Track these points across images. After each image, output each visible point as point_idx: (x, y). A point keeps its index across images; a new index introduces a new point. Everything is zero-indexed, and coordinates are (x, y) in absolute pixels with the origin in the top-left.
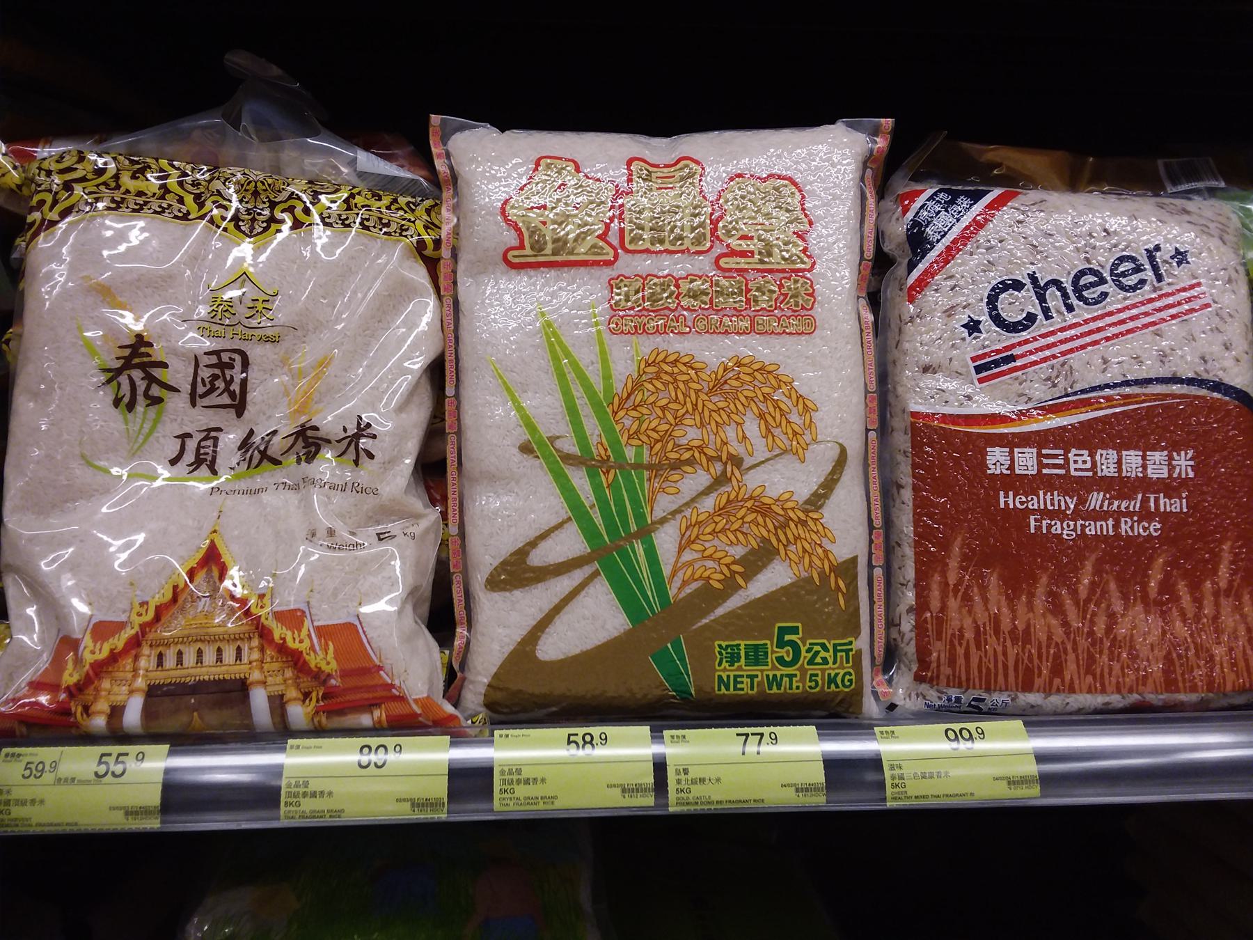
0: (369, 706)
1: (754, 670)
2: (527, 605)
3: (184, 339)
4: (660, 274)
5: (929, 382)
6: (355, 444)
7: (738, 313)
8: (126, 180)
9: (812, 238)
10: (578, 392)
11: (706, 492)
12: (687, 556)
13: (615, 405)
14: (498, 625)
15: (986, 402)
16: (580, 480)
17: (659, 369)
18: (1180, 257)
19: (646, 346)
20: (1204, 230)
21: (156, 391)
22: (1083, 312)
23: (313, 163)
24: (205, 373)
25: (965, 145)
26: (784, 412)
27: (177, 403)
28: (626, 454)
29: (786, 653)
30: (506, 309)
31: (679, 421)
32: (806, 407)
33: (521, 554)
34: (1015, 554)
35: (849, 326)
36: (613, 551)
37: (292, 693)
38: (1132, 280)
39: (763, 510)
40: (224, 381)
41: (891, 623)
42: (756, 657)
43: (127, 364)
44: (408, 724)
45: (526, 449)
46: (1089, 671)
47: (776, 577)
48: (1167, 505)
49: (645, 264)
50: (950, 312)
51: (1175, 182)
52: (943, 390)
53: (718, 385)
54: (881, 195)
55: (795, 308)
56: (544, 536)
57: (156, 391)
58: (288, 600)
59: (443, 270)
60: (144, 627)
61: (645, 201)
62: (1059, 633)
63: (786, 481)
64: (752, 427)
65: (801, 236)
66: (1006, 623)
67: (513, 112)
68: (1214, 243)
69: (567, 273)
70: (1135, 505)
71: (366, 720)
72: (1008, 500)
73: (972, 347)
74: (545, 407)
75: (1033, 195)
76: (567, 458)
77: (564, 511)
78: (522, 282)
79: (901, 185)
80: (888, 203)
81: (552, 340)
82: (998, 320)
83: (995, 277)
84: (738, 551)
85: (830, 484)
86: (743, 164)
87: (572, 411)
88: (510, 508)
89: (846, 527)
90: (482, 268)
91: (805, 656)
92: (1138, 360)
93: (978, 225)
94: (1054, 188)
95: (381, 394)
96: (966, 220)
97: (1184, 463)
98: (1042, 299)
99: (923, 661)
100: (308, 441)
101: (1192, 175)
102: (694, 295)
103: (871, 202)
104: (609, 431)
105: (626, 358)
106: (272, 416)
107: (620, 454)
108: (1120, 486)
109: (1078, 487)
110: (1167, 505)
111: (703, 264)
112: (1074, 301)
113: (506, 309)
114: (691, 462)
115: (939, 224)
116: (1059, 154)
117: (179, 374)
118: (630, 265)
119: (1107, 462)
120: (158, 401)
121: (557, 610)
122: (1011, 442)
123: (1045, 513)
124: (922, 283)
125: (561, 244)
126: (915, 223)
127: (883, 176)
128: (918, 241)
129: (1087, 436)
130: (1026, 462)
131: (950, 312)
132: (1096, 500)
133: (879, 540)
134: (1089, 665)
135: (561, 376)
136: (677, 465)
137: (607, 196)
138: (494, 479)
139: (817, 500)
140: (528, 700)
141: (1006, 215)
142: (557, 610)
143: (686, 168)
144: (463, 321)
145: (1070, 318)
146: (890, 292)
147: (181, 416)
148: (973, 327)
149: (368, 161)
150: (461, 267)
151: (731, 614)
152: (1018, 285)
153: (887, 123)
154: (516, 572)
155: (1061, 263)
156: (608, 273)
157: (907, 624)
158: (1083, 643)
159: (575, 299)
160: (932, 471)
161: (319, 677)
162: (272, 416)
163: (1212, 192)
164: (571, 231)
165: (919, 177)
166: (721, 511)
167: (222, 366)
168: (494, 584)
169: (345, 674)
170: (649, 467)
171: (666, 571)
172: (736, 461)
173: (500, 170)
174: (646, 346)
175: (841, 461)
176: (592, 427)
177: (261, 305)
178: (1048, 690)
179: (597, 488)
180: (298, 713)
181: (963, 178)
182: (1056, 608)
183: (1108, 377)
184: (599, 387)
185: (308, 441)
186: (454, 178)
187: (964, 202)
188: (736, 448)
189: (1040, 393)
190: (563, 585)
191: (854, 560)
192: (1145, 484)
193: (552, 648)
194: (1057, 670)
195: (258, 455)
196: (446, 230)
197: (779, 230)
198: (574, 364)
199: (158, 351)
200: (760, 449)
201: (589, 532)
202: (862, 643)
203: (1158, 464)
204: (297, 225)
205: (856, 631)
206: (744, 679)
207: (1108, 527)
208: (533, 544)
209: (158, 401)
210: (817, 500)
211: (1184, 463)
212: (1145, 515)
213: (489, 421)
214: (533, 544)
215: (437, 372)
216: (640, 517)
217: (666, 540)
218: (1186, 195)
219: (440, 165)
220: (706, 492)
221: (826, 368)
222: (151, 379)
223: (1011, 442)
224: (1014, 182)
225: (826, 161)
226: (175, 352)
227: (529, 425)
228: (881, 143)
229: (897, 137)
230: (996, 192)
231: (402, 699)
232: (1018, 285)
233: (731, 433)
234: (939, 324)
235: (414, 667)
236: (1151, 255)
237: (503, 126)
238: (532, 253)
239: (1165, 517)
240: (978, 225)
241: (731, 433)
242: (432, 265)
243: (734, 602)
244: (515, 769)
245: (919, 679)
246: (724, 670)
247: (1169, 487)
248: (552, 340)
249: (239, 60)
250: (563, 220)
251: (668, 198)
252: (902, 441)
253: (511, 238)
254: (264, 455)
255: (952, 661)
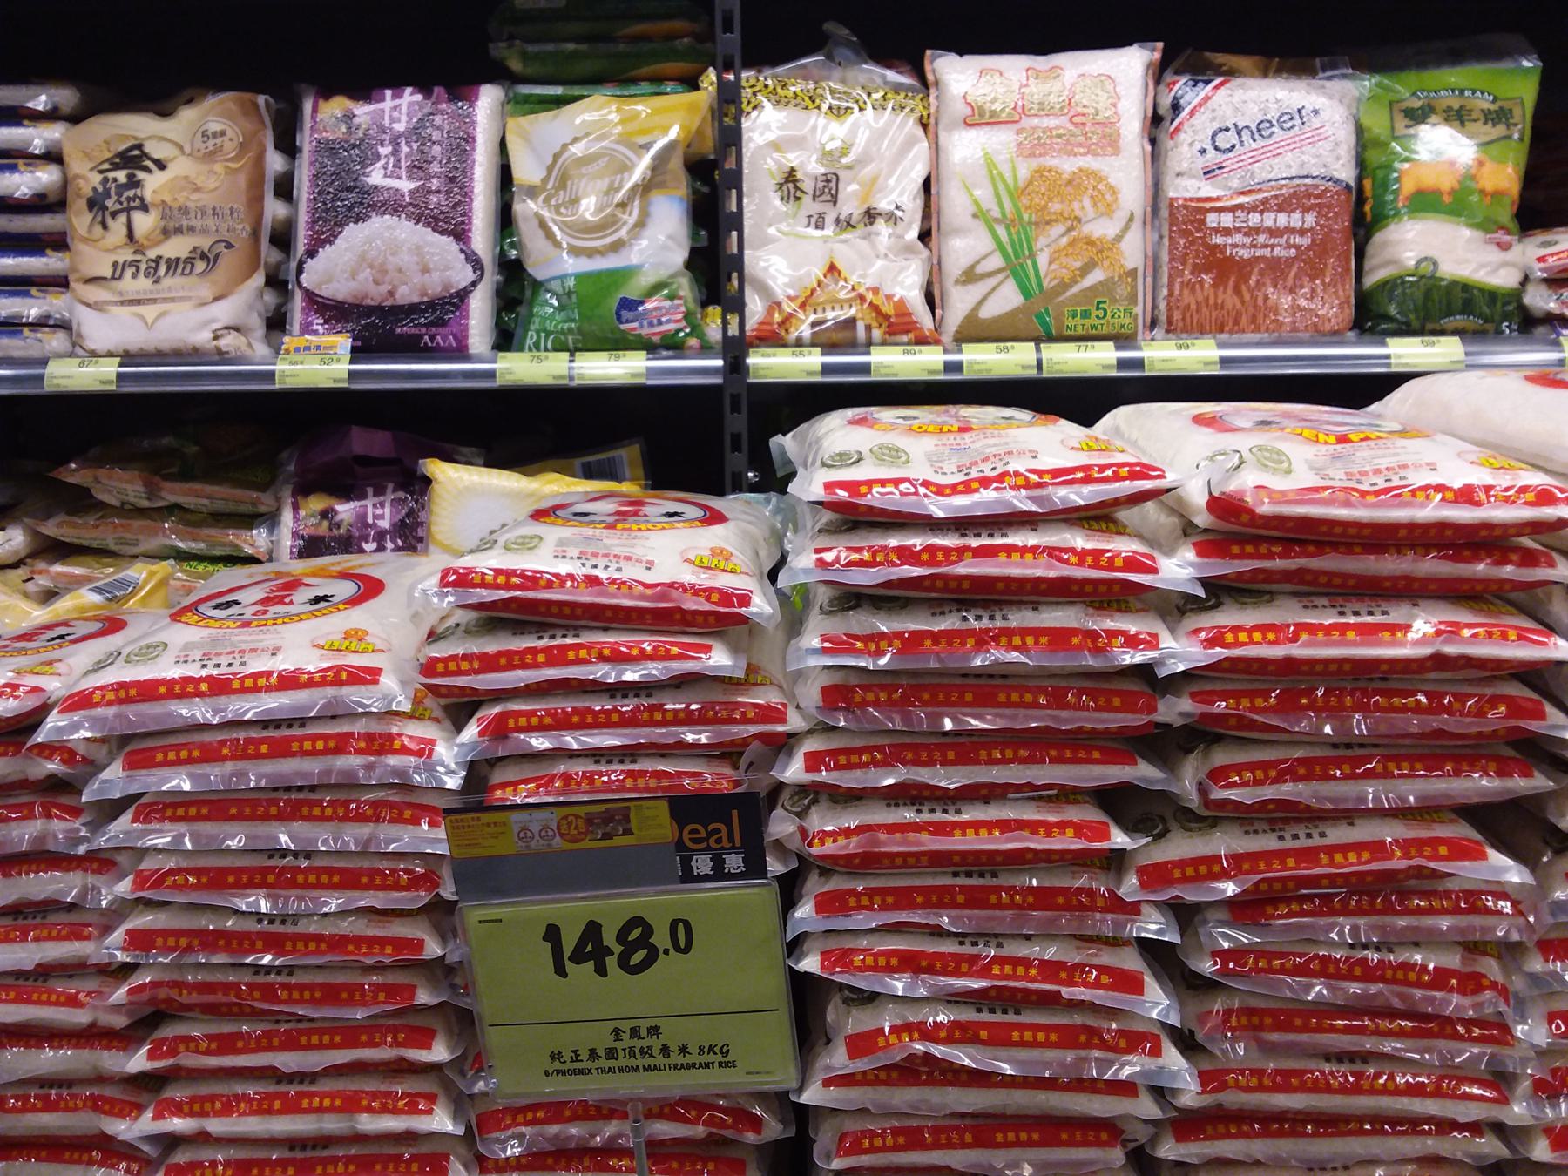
0: (907, 332)
1: (1086, 321)
2: (975, 292)
3: (811, 167)
4: (165, 567)
5: (1178, 180)
6: (891, 218)
7: (1081, 145)
8: (779, 90)
9: (1119, 106)
10: (1001, 187)
11: (1063, 235)
12: (1053, 267)
13: (1018, 193)
14: (959, 303)
15: (1207, 190)
16: (1001, 231)
17: (1040, 172)
18: (1316, 112)
19: (1034, 163)
20: (1331, 97)
21: (799, 194)
22: (1261, 143)
23: (862, 78)
24: (820, 185)
25: (1208, 54)
26: (1105, 200)
27: (807, 199)
28: (1024, 214)
29: (1101, 313)
30: (964, 147)
31: (1050, 199)
32: (1114, 191)
33: (972, 267)
34: (1223, 267)
35: (1137, 150)
36: (1017, 266)
37: (875, 324)
38: (1290, 124)
39: (1090, 243)
40: (829, 188)
41: (1155, 307)
42: (1086, 315)
43: (787, 181)
44: (922, 341)
45: (975, 216)
46: (1253, 322)
47: (1096, 276)
48: (1299, 240)
49: (1036, 121)
50: (1191, 145)
51: (1324, 70)
52: (1185, 188)
53: (1070, 182)
54: (1158, 82)
55: (1111, 143)
56: (983, 258)
57: (799, 194)
58: (869, 283)
59: (931, 128)
60: (807, 298)
61: (1036, 90)
62: (1239, 305)
63: (1104, 229)
64: (1087, 203)
65: (1114, 105)
66: (1212, 302)
67: (966, 45)
68: (1335, 103)
69: (996, 127)
70: (1282, 241)
71: (905, 338)
72: (1217, 240)
73: (1201, 162)
74: (983, 193)
75: (1239, 81)
76: (996, 220)
77: (994, 246)
78: (973, 133)
79: (1168, 77)
80: (1162, 87)
81: (989, 163)
82: (1216, 148)
83: (1216, 126)
84: (1078, 264)
85: (1126, 228)
86: (1085, 69)
87: (998, 196)
88: (965, 246)
89: (1133, 251)
90: (952, 127)
91: (1109, 314)
92: (1289, 166)
93: (1207, 98)
94: (1252, 76)
95: (901, 193)
96: (1202, 95)
97: (1311, 219)
98: (1239, 133)
99: (1170, 322)
100: (871, 215)
101: (1334, 66)
102: (1059, 136)
103: (1151, 87)
104: (1015, 206)
105: (1024, 172)
106: (850, 205)
107: (1021, 218)
108: (1274, 232)
109: (1252, 231)
110: (1299, 240)
111: (1063, 121)
112: (1257, 136)
113: (964, 147)
114: (1056, 221)
115: (1187, 98)
116: (1256, 58)
117: (808, 185)
118: (1027, 122)
119: (1269, 220)
120: (798, 199)
121: (989, 294)
122: (1220, 210)
123: (1235, 246)
124: (1177, 129)
125: (993, 113)
126: (1175, 98)
127: (1159, 73)
128: (1176, 107)
129: (1262, 207)
130: (1227, 220)
131: (1191, 145)
132: (1262, 239)
133: (1150, 263)
134: (1253, 320)
135: (993, 178)
136: (1048, 223)
137: (1016, 87)
138: (958, 231)
139: (1118, 239)
140: (975, 332)
141: (1222, 91)
142: (989, 294)
143: (1054, 73)
144: (941, 154)
145: (1254, 145)
146: (1163, 138)
147: (809, 206)
148: (1203, 151)
149: (891, 75)
150: (940, 127)
151: (1075, 295)
152: (1227, 129)
153: (1160, 45)
154: (970, 276)
155: (1250, 118)
156: (1016, 126)
157: (1163, 305)
158: (1251, 310)
159: (999, 141)
160: (1180, 224)
161: (887, 317)
162: (850, 205)
163: (1344, 76)
164: (997, 106)
165: (1178, 72)
166: (1072, 244)
167: (828, 181)
168: (957, 282)
169: (897, 315)
170: (1037, 224)
171: (1042, 274)
172: (1079, 220)
173: (961, 76)
174: (1034, 163)
175: (1131, 219)
176: (1008, 205)
177: (844, 151)
178: (1231, 332)
179: (1010, 234)
180: (877, 334)
181: (1201, 71)
182: (1237, 291)
183: (1271, 176)
184: (1010, 181)
185: (871, 215)
186: (937, 83)
187: (1201, 85)
188: (1078, 213)
189: (1235, 184)
190: (992, 282)
191: (1135, 270)
192: (1289, 230)
193: (987, 312)
194: (1236, 322)
195: (845, 224)
196: (932, 110)
197: (1103, 101)
198: (1000, 174)
199: (799, 175)
200: (1091, 212)
201: (1005, 256)
202: (1138, 310)
203: (1296, 220)
204: (861, 109)
205: (1135, 303)
206: (1080, 325)
207: (1267, 252)
208: (978, 262)
209: (798, 199)
210: (1118, 239)
211: (1311, 219)
212: (1289, 246)
213: (955, 202)
214: (978, 262)
215: (927, 184)
216: (1030, 248)
217: (1042, 260)
218: (1329, 78)
219: (930, 77)
220: (1063, 235)
221: (1126, 173)
222: (797, 188)
223: (1220, 210)
224: (1231, 73)
225: (1128, 66)
226: (806, 174)
227: (976, 202)
228: (1157, 56)
229: (1165, 52)
230: (1219, 80)
231: (921, 329)
232: (1227, 129)
233: (1076, 205)
234: (1186, 149)
235: (925, 320)
236: (1299, 111)
237: (961, 54)
238: (979, 118)
239: (1297, 247)
240: (1207, 98)
241: (1076, 205)
242: (925, 126)
243: (1075, 289)
244: (970, 363)
245: (1168, 331)
246: (1070, 322)
247: (1302, 232)
248: (989, 163)
249: (829, 26)
250: (994, 101)
251: (1046, 87)
252: (1164, 213)
253: (968, 111)
254: (848, 224)
255: (1184, 319)
